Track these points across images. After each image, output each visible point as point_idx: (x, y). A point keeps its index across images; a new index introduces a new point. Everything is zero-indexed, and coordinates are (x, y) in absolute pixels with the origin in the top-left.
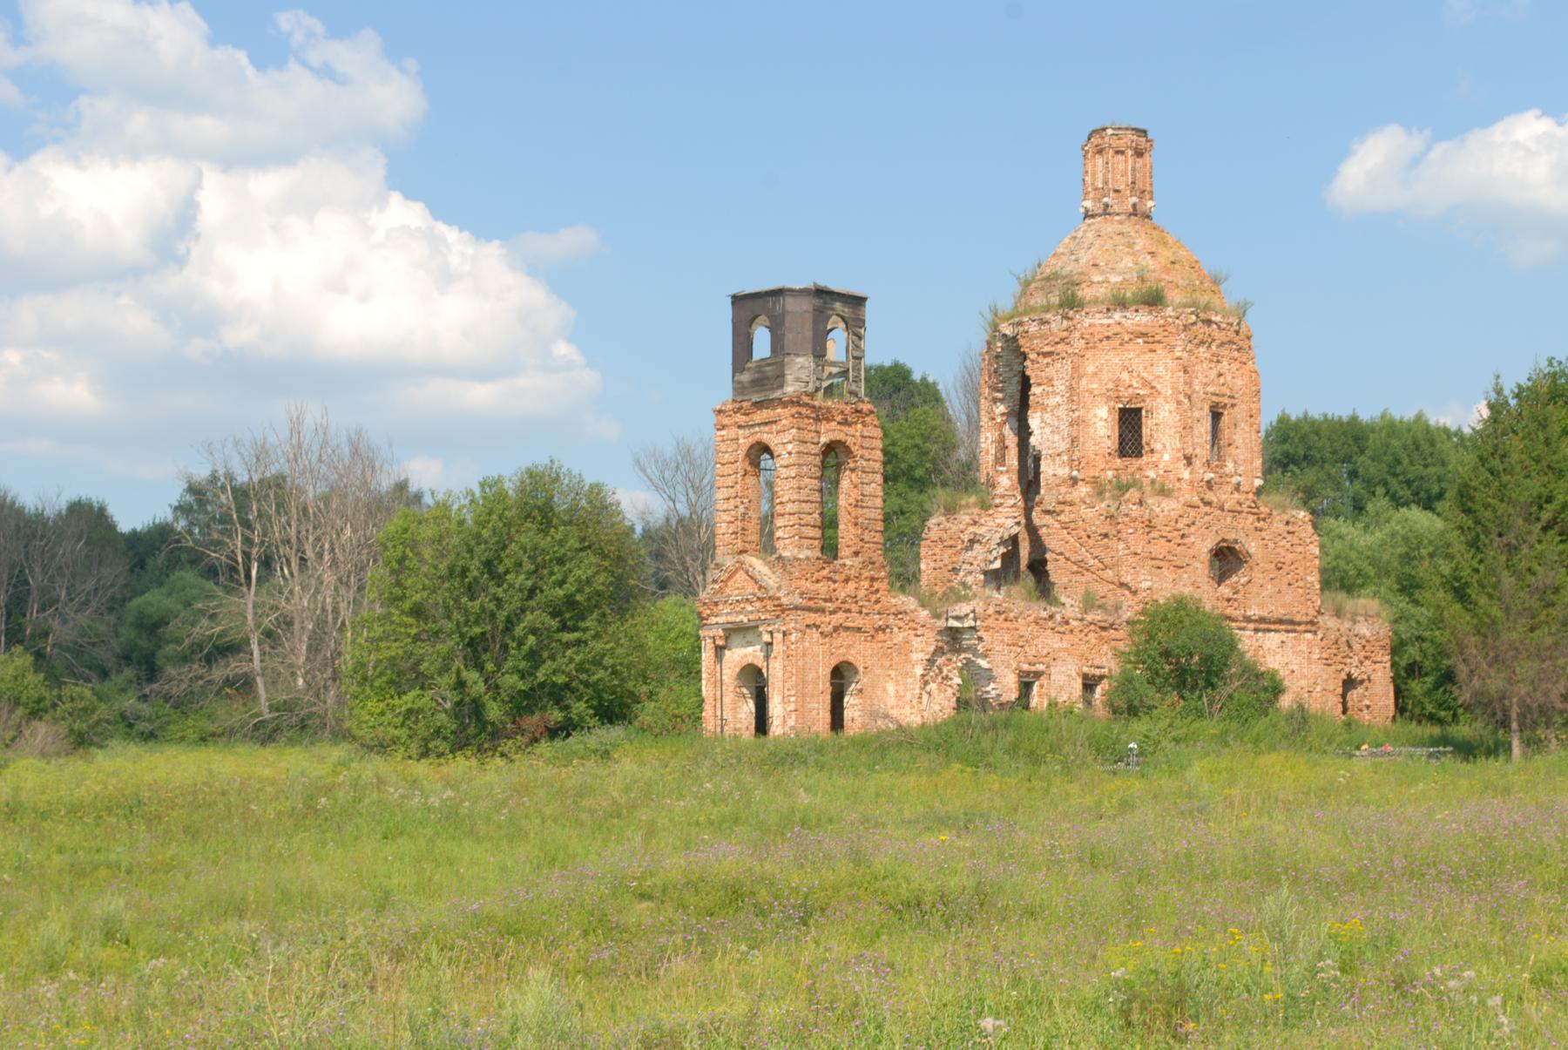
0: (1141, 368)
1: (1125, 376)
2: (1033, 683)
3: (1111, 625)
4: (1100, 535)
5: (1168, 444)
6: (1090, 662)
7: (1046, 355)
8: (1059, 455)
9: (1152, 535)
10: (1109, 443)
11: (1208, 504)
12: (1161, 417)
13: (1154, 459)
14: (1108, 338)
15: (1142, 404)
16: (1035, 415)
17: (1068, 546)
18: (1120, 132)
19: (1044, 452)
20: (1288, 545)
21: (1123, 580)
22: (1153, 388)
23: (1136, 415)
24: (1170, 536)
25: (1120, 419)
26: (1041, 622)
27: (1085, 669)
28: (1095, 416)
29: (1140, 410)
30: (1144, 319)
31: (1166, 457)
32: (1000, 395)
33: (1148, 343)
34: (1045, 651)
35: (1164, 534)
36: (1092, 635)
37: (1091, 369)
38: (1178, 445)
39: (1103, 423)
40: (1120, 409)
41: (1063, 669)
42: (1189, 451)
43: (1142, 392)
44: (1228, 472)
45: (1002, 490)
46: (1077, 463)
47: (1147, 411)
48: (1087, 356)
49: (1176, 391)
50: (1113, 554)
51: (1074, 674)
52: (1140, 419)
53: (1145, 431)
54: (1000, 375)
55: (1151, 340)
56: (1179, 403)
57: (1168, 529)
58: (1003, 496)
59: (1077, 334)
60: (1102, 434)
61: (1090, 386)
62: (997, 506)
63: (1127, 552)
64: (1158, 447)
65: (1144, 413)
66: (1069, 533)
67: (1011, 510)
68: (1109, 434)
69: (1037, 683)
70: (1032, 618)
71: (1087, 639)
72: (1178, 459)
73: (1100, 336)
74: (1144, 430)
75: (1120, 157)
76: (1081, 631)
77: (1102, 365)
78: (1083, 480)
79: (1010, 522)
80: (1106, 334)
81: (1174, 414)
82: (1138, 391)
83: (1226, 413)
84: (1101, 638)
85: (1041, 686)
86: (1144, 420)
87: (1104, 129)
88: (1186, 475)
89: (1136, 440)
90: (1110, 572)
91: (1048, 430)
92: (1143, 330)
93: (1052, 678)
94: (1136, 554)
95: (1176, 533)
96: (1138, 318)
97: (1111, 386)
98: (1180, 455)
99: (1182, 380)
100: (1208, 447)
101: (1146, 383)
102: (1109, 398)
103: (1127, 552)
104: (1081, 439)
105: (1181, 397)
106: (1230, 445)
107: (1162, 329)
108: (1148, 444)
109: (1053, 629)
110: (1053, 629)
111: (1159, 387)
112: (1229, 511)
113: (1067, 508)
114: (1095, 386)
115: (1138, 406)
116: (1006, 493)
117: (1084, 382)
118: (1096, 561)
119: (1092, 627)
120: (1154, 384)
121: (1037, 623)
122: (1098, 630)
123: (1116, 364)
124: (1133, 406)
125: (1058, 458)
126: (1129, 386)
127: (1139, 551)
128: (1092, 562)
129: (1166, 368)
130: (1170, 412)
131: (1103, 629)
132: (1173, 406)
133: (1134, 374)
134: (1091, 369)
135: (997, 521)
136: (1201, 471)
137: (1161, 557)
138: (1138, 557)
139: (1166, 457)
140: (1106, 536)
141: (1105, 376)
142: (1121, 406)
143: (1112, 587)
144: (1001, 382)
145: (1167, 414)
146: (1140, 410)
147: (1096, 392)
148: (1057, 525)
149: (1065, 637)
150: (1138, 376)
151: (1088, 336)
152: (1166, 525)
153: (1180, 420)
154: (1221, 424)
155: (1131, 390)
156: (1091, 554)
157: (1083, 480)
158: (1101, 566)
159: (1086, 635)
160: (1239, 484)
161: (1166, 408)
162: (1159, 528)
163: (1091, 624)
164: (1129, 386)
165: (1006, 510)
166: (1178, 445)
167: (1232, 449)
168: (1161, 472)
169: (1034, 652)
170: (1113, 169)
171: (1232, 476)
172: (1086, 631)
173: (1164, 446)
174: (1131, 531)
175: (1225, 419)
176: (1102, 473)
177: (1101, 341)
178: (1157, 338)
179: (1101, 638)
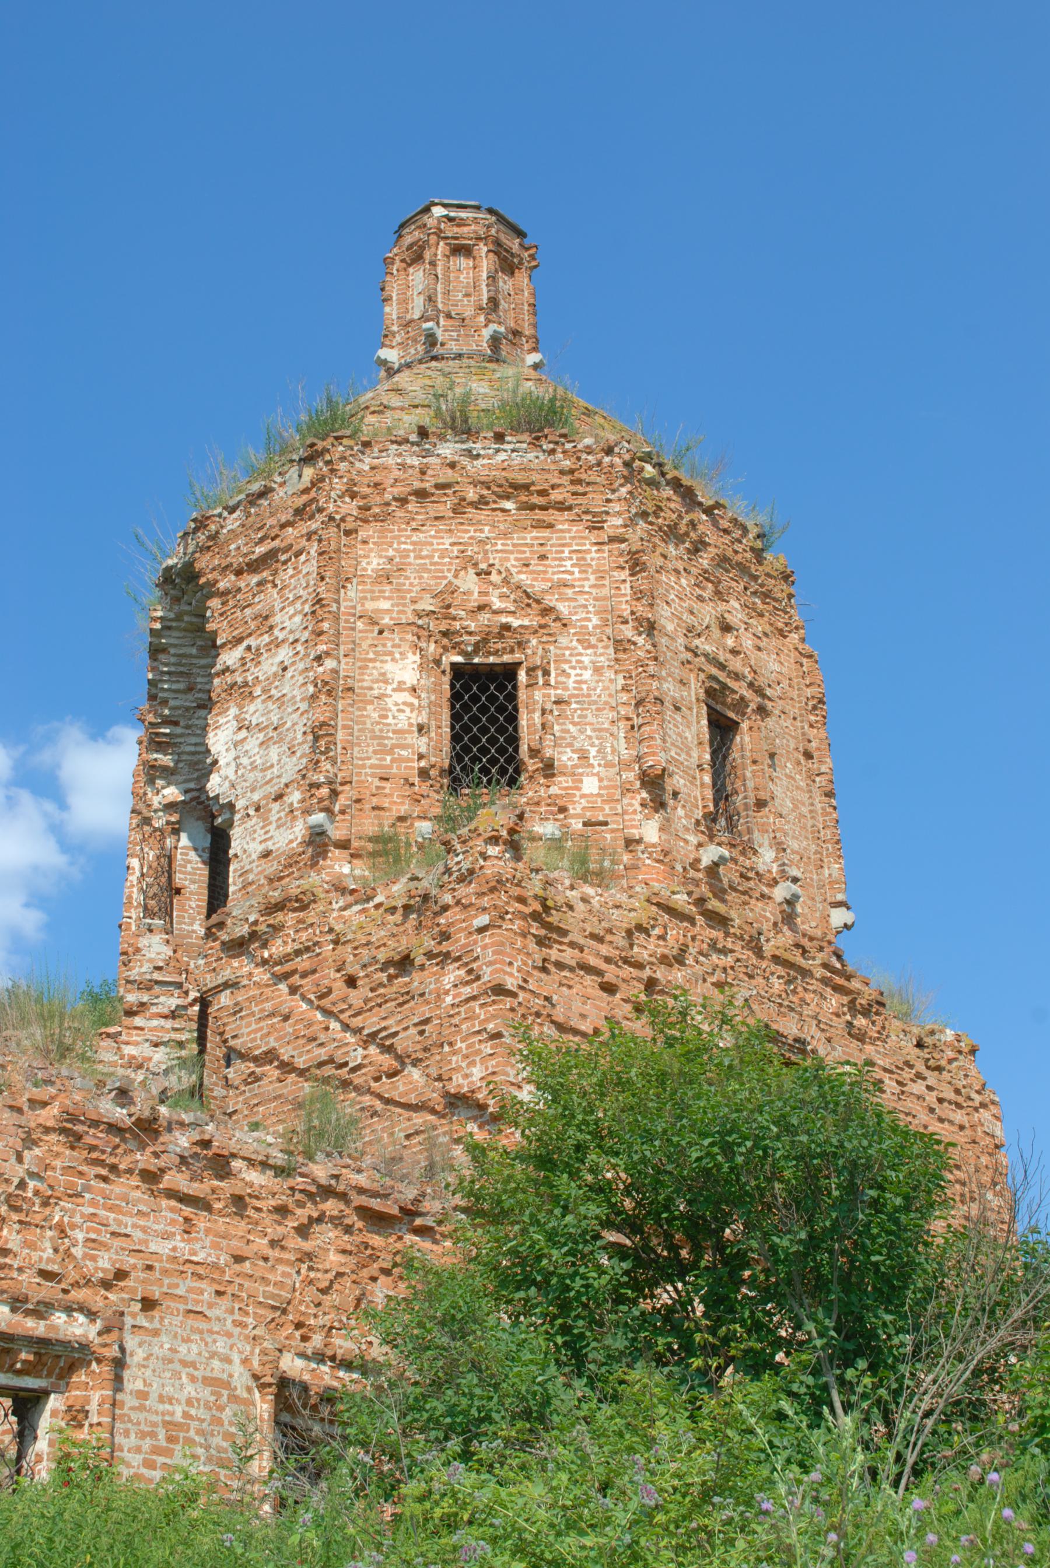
0: (512, 563)
1: (469, 582)
2: (45, 1393)
3: (409, 1213)
4: (388, 963)
5: (593, 752)
6: (317, 1340)
7: (254, 567)
8: (279, 797)
9: (554, 954)
10: (422, 744)
11: (719, 921)
12: (571, 684)
13: (554, 790)
14: (421, 494)
15: (518, 656)
16: (222, 720)
17: (289, 1028)
18: (463, 214)
19: (239, 805)
20: (931, 1098)
21: (459, 1083)
22: (547, 611)
23: (501, 688)
24: (611, 973)
25: (455, 697)
26: (94, 1137)
27: (292, 1365)
28: (384, 679)
29: (509, 672)
30: (517, 459)
31: (590, 785)
32: (166, 760)
33: (532, 507)
34: (105, 1262)
35: (593, 961)
36: (327, 1235)
37: (373, 563)
38: (625, 753)
39: (406, 697)
40: (453, 665)
41: (190, 1351)
42: (656, 760)
43: (516, 623)
44: (761, 868)
45: (146, 967)
46: (325, 791)
47: (531, 671)
48: (362, 534)
49: (611, 617)
50: (425, 1011)
51: (240, 1378)
52: (512, 697)
53: (527, 721)
54: (164, 702)
55: (536, 500)
56: (621, 645)
57: (605, 950)
58: (147, 986)
59: (339, 485)
60: (403, 725)
61: (370, 605)
62: (130, 1013)
63: (467, 991)
64: (566, 758)
65: (522, 676)
66: (293, 990)
67: (169, 1024)
68: (423, 718)
69: (54, 1402)
70: (49, 1115)
71: (307, 1246)
72: (627, 790)
73: (398, 491)
74: (523, 721)
75: (464, 262)
76: (282, 1211)
77: (405, 554)
78: (344, 845)
79: (159, 1057)
80: (417, 485)
81: (610, 674)
82: (504, 619)
83: (744, 726)
84: (366, 1255)
85: (76, 1416)
86: (522, 695)
87: (427, 210)
88: (650, 831)
89: (502, 751)
90: (415, 1074)
91: (252, 744)
92: (521, 478)
93: (133, 1380)
94: (500, 990)
95: (628, 971)
96: (502, 456)
97: (427, 604)
98: (631, 776)
99: (626, 589)
100: (707, 779)
101: (528, 599)
102: (421, 632)
103: (467, 991)
104: (340, 735)
105: (628, 631)
106: (761, 804)
107: (568, 478)
108: (534, 753)
109: (150, 1177)
110: (150, 1177)
111: (563, 608)
112: (776, 959)
113: (289, 918)
114: (385, 605)
115: (507, 658)
116: (157, 976)
117: (352, 592)
118: (373, 1050)
119: (331, 1206)
120: (550, 600)
121: (75, 1139)
122: (353, 1219)
123: (443, 554)
124: (492, 659)
125: (276, 806)
126: (481, 608)
127: (511, 984)
128: (357, 1056)
129: (582, 565)
130: (597, 670)
131: (377, 1220)
132: (605, 655)
133: (494, 577)
134: (373, 563)
135: (128, 1050)
136: (693, 839)
137: (586, 1027)
138: (509, 1002)
139: (590, 785)
140: (404, 963)
141: (411, 581)
142: (459, 659)
143: (419, 1119)
144: (167, 722)
145: (587, 675)
146: (509, 672)
147: (386, 621)
148: (261, 975)
149: (202, 1221)
150: (506, 581)
151: (366, 490)
152: (600, 939)
153: (625, 689)
154: (735, 754)
155: (484, 617)
156: (358, 1031)
157: (344, 845)
158: (387, 1061)
159: (303, 1231)
160: (791, 902)
161: (586, 660)
162: (575, 936)
163: (327, 1192)
164: (481, 608)
165: (155, 1023)
166: (625, 753)
167: (767, 816)
168: (577, 825)
169: (45, 1255)
170: (448, 281)
171: (775, 882)
172: (302, 1214)
173: (584, 757)
174: (483, 920)
175: (744, 740)
176: (401, 828)
177: (403, 501)
178: (556, 496)
179: (366, 1255)
